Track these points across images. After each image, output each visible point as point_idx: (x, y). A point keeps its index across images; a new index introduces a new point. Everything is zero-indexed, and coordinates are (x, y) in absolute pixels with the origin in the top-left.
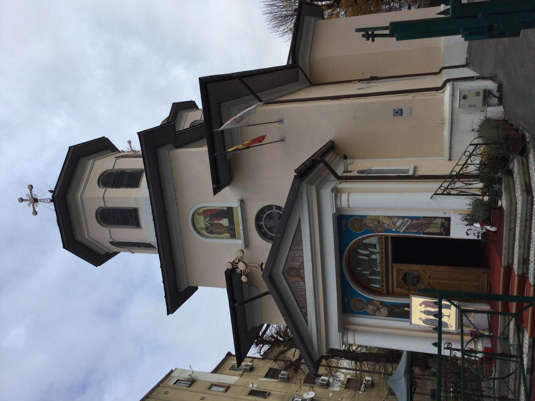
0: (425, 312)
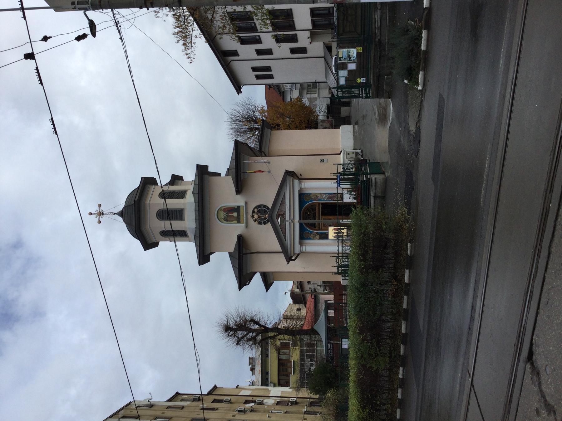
0: (334, 233)
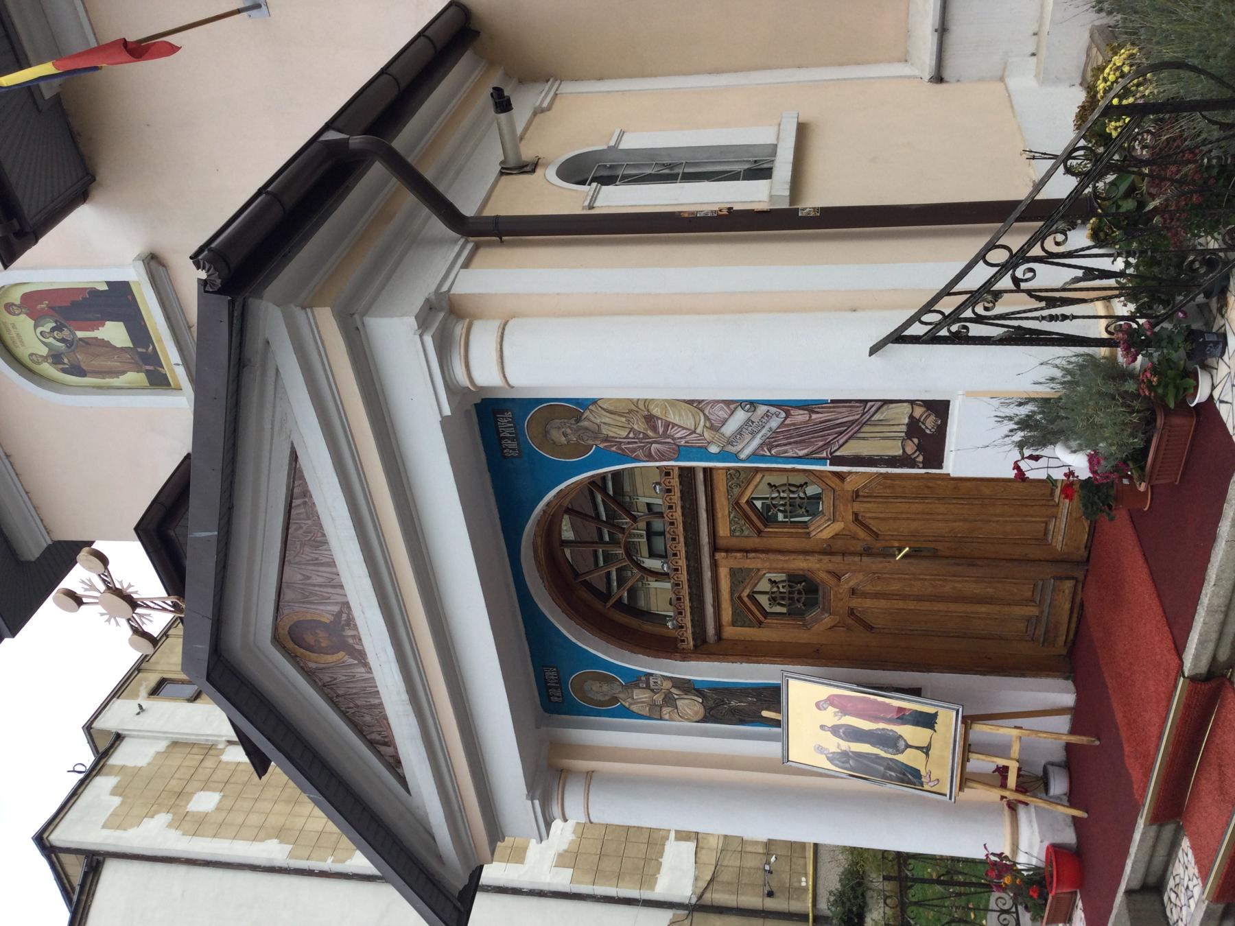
0: (835, 730)
